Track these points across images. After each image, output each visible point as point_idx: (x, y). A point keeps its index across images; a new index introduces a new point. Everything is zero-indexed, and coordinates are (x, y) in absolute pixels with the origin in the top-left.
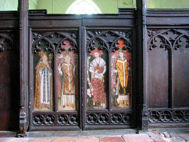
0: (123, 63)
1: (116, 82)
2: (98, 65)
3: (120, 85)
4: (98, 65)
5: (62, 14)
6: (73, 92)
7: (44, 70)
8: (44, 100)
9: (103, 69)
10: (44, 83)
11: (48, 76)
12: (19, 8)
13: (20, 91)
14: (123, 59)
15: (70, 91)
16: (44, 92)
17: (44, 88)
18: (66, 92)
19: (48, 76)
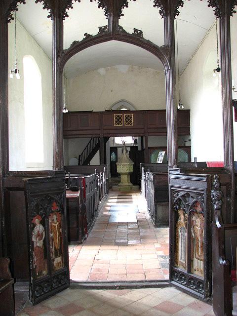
0: (56, 225)
1: (53, 246)
2: (39, 232)
3: (55, 249)
4: (39, 232)
5: (42, 119)
6: (202, 258)
7: (181, 229)
8: (181, 259)
9: (42, 235)
10: (182, 242)
11: (184, 236)
12: (224, 231)
13: (39, 68)
14: (56, 221)
15: (200, 256)
16: (181, 251)
17: (182, 246)
18: (197, 256)
19: (184, 236)
